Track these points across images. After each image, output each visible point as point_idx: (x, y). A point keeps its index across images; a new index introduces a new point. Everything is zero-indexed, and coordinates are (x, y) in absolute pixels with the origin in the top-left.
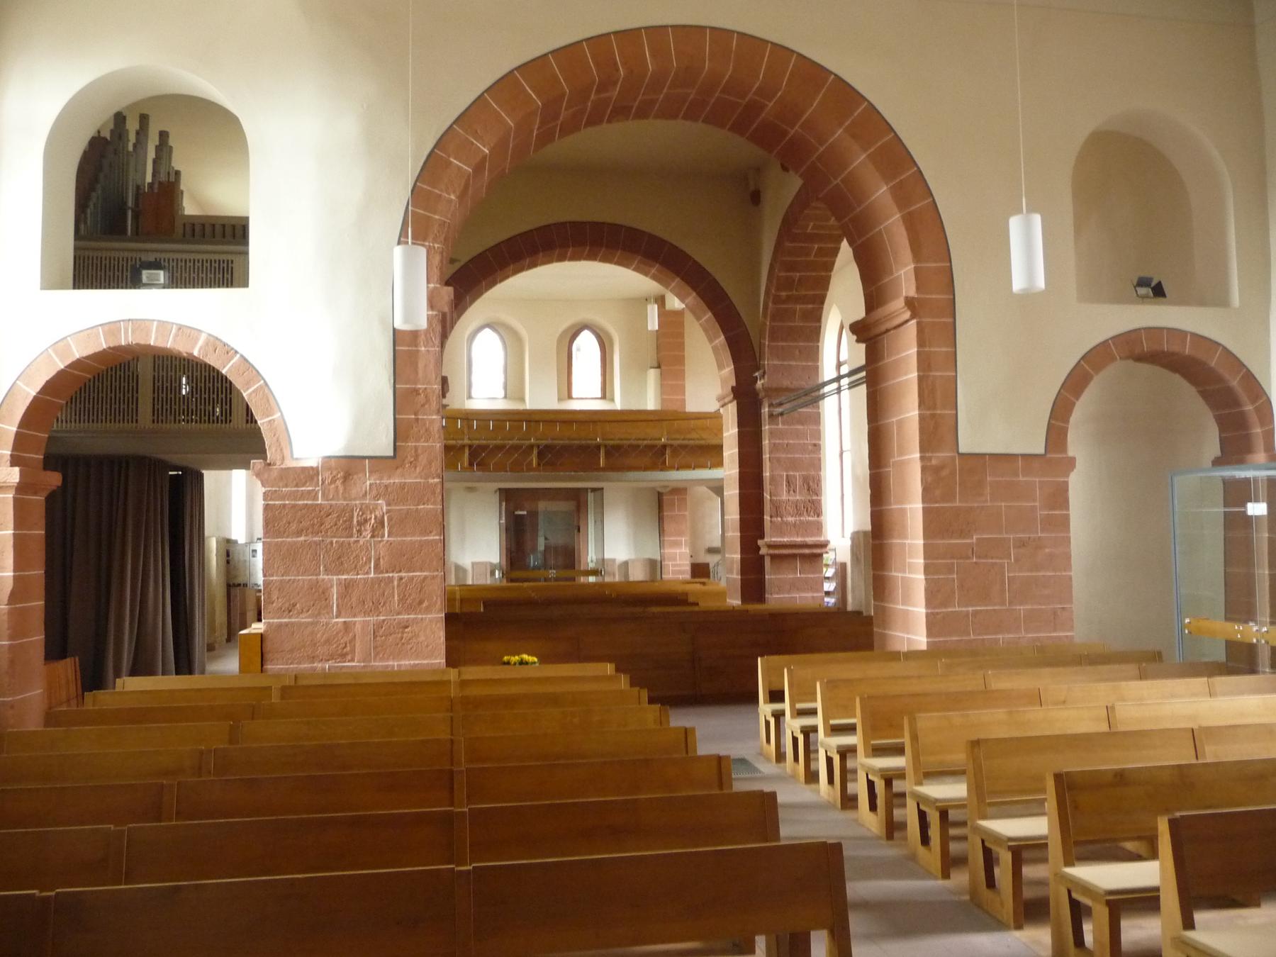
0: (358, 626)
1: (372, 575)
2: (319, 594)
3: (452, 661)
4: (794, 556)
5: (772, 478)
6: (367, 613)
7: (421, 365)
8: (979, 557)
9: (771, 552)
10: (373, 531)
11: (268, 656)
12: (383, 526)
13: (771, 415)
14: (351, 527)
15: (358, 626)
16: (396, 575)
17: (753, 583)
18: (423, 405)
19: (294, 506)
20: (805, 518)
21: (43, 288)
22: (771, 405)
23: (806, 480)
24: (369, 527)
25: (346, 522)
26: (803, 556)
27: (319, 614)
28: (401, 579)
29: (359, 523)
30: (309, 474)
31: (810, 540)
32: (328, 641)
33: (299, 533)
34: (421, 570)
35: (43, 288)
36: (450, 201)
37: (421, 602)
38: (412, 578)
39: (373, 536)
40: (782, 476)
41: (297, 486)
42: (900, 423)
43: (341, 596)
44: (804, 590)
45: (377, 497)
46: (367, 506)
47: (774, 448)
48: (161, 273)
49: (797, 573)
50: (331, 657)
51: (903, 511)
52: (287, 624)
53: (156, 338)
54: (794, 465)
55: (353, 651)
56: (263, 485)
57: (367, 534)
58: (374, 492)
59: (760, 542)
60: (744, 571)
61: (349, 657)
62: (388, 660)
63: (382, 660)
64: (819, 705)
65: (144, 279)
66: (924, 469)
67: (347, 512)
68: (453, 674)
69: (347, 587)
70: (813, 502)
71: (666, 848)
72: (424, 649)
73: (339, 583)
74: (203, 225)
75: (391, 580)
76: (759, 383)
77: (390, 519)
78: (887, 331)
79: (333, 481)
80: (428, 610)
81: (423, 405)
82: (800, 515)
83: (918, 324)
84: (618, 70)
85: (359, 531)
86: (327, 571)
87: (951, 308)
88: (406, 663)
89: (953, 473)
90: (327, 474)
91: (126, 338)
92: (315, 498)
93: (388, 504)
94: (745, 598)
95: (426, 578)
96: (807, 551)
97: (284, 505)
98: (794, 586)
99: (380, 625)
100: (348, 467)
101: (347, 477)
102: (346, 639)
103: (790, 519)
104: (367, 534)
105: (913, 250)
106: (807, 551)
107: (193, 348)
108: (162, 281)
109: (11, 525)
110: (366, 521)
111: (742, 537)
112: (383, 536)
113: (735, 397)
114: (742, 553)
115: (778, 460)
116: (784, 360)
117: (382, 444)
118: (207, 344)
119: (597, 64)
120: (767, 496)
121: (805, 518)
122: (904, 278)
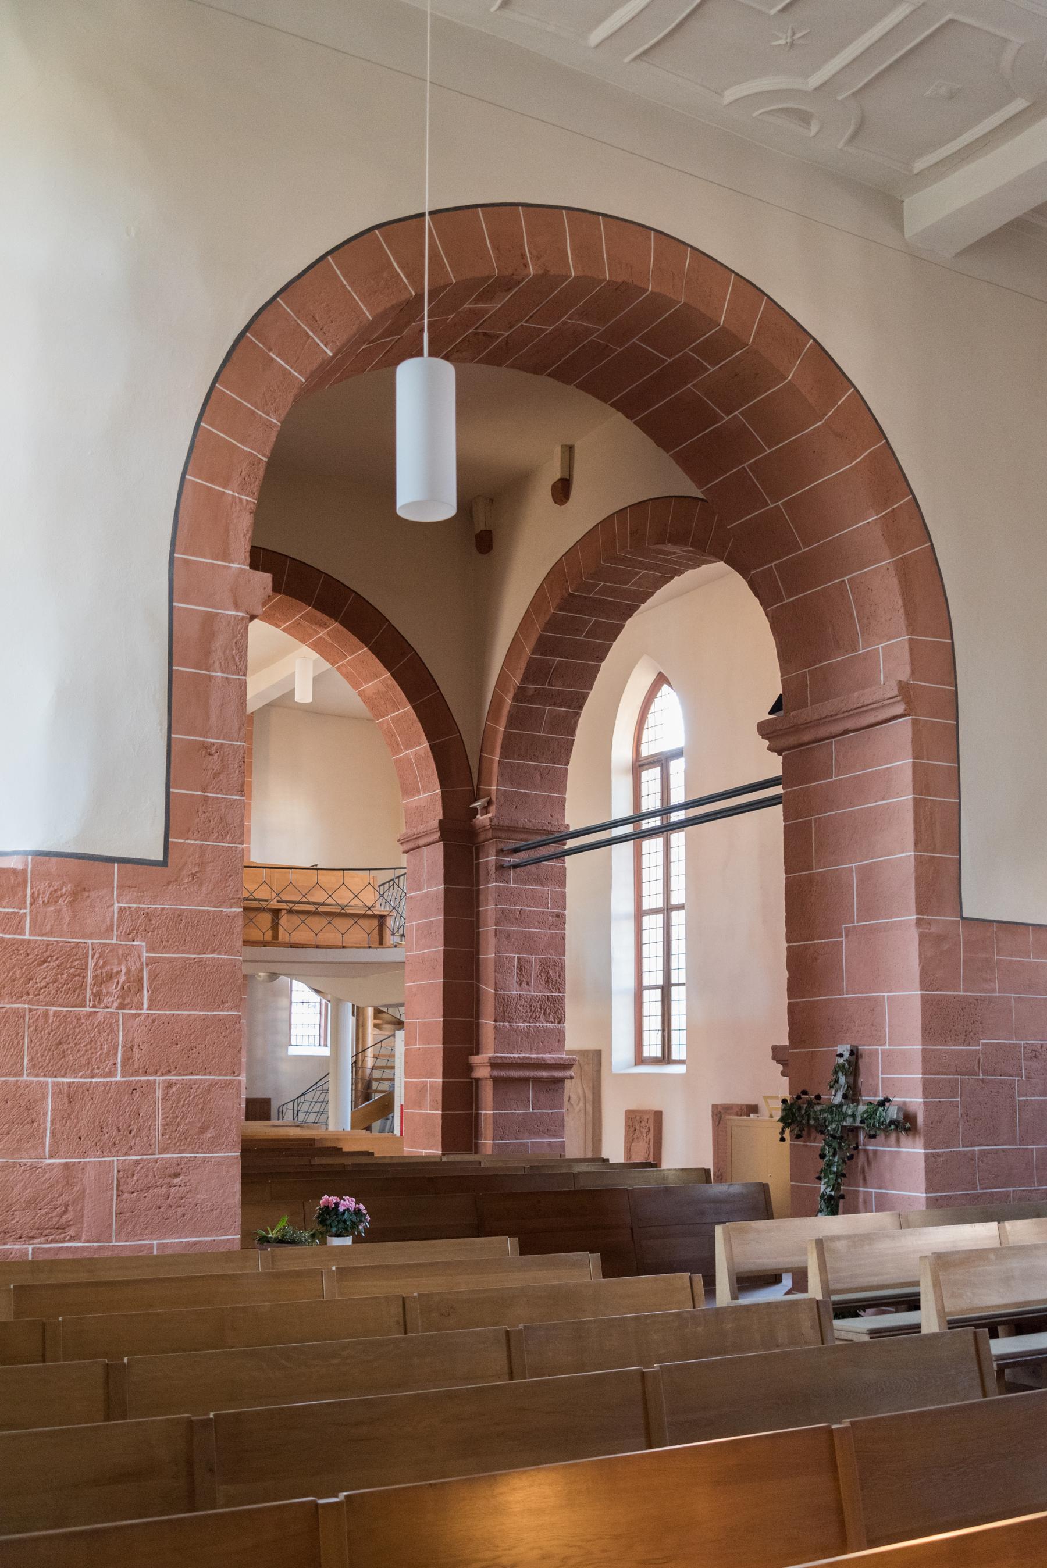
0: (90, 1174)
3: (254, 1238)
4: (526, 1080)
5: (499, 964)
6: (111, 1148)
7: (215, 703)
8: (985, 1073)
9: (496, 1073)
13: (500, 867)
14: (82, 987)
15: (90, 1174)
17: (460, 1120)
18: (216, 775)
20: (543, 1024)
22: (500, 852)
23: (544, 965)
24: (113, 988)
25: (67, 973)
26: (538, 1081)
28: (170, 1085)
29: (99, 981)
31: (549, 1057)
32: (33, 1202)
34: (205, 1071)
36: (269, 425)
37: (203, 1129)
38: (190, 1085)
40: (511, 959)
42: (867, 874)
43: (63, 1116)
44: (538, 1134)
45: (131, 934)
46: (114, 948)
47: (503, 916)
49: (526, 1107)
50: (41, 1232)
51: (873, 1006)
54: (528, 943)
55: (79, 1218)
57: (112, 1000)
58: (127, 925)
59: (475, 1059)
60: (448, 1102)
61: (72, 1232)
62: (141, 1236)
63: (132, 1235)
66: (923, 938)
67: (74, 955)
68: (260, 1260)
69: (71, 1097)
70: (553, 1000)
72: (207, 1215)
76: (482, 819)
77: (153, 977)
78: (846, 732)
79: (53, 900)
80: (214, 1144)
81: (216, 775)
82: (536, 1019)
83: (915, 722)
84: (526, 266)
85: (97, 995)
86: (35, 1068)
87: (952, 704)
88: (176, 1242)
89: (957, 944)
90: (43, 886)
92: (19, 929)
93: (151, 949)
94: (448, 1145)
95: (213, 1085)
96: (545, 1074)
98: (526, 1126)
99: (126, 1173)
102: (66, 1198)
103: (522, 1025)
104: (112, 1000)
105: (907, 613)
106: (545, 1074)
110: (110, 976)
111: (446, 1051)
112: (140, 1006)
113: (443, 838)
114: (445, 1075)
115: (508, 935)
116: (518, 785)
119: (497, 249)
120: (488, 990)
121: (543, 1024)
122: (886, 657)
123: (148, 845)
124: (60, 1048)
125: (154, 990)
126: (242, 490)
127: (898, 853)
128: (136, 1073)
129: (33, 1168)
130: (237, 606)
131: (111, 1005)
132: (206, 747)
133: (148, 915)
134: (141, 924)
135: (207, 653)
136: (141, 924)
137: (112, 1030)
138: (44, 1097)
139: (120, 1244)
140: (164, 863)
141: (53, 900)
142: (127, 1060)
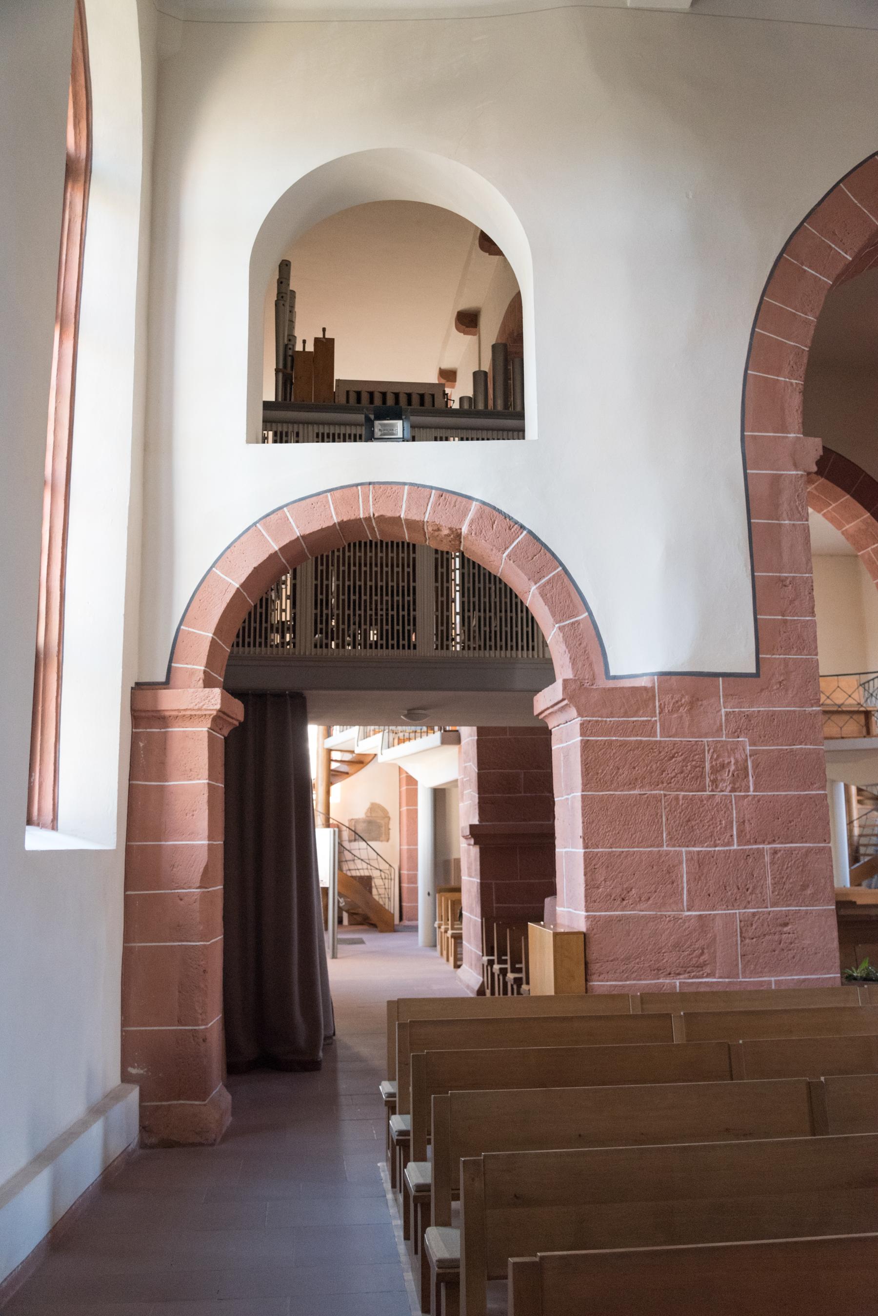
0: (719, 924)
1: (665, 848)
2: (666, 872)
6: (732, 903)
10: (735, 778)
11: (595, 967)
12: (747, 776)
14: (702, 776)
15: (719, 924)
16: (767, 847)
18: (792, 602)
19: (624, 744)
21: (248, 441)
25: (689, 766)
27: (664, 904)
29: (715, 770)
30: (636, 698)
32: (676, 945)
33: (631, 784)
34: (802, 839)
35: (248, 441)
36: (807, 322)
37: (804, 887)
38: (791, 851)
39: (733, 790)
41: (626, 715)
43: (696, 878)
45: (736, 733)
48: (399, 423)
50: (683, 969)
52: (620, 919)
53: (408, 509)
56: (580, 714)
61: (708, 970)
62: (761, 973)
64: (508, 958)
65: (377, 434)
67: (693, 752)
69: (700, 862)
71: (161, 1030)
73: (691, 857)
74: (384, 395)
75: (760, 852)
77: (756, 766)
79: (675, 709)
91: (365, 508)
95: (809, 851)
97: (611, 743)
99: (747, 922)
100: (691, 688)
101: (693, 703)
102: (701, 942)
104: (726, 785)
107: (461, 521)
108: (400, 435)
109: (205, 772)
110: (723, 766)
112: (748, 790)
117: (740, 657)
118: (480, 516)
123: (740, 657)
124: (690, 824)
125: (757, 776)
126: (791, 375)
127: (318, 967)
128: (748, 843)
129: (676, 919)
130: (796, 467)
131: (725, 790)
132: (782, 580)
133: (748, 717)
134: (743, 724)
135: (777, 506)
136: (743, 724)
137: (728, 809)
138: (681, 863)
139: (746, 980)
140: (757, 675)
141: (675, 709)
142: (741, 832)
